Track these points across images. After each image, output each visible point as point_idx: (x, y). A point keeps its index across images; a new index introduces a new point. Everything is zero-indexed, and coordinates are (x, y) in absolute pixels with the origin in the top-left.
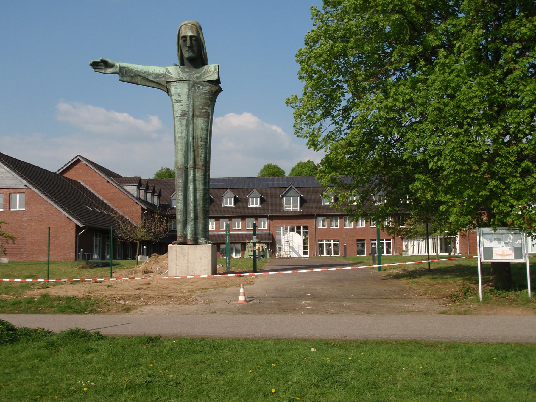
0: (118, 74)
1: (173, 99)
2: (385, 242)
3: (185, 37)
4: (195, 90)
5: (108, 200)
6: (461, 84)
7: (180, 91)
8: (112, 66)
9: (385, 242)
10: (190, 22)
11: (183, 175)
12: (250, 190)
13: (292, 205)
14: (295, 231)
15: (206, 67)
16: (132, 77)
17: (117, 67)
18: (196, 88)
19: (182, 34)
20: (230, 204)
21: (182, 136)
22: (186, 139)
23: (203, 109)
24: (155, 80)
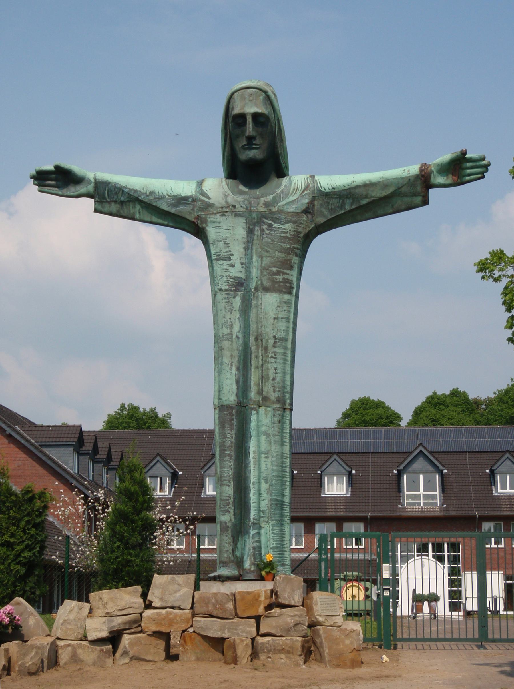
1: (213, 252)
3: (242, 117)
4: (262, 231)
7: (229, 232)
10: (245, 85)
11: (235, 422)
13: (422, 492)
14: (431, 553)
15: (285, 181)
16: (122, 203)
17: (89, 182)
18: (265, 227)
19: (237, 111)
21: (231, 334)
22: (241, 341)
23: (278, 273)
24: (173, 210)
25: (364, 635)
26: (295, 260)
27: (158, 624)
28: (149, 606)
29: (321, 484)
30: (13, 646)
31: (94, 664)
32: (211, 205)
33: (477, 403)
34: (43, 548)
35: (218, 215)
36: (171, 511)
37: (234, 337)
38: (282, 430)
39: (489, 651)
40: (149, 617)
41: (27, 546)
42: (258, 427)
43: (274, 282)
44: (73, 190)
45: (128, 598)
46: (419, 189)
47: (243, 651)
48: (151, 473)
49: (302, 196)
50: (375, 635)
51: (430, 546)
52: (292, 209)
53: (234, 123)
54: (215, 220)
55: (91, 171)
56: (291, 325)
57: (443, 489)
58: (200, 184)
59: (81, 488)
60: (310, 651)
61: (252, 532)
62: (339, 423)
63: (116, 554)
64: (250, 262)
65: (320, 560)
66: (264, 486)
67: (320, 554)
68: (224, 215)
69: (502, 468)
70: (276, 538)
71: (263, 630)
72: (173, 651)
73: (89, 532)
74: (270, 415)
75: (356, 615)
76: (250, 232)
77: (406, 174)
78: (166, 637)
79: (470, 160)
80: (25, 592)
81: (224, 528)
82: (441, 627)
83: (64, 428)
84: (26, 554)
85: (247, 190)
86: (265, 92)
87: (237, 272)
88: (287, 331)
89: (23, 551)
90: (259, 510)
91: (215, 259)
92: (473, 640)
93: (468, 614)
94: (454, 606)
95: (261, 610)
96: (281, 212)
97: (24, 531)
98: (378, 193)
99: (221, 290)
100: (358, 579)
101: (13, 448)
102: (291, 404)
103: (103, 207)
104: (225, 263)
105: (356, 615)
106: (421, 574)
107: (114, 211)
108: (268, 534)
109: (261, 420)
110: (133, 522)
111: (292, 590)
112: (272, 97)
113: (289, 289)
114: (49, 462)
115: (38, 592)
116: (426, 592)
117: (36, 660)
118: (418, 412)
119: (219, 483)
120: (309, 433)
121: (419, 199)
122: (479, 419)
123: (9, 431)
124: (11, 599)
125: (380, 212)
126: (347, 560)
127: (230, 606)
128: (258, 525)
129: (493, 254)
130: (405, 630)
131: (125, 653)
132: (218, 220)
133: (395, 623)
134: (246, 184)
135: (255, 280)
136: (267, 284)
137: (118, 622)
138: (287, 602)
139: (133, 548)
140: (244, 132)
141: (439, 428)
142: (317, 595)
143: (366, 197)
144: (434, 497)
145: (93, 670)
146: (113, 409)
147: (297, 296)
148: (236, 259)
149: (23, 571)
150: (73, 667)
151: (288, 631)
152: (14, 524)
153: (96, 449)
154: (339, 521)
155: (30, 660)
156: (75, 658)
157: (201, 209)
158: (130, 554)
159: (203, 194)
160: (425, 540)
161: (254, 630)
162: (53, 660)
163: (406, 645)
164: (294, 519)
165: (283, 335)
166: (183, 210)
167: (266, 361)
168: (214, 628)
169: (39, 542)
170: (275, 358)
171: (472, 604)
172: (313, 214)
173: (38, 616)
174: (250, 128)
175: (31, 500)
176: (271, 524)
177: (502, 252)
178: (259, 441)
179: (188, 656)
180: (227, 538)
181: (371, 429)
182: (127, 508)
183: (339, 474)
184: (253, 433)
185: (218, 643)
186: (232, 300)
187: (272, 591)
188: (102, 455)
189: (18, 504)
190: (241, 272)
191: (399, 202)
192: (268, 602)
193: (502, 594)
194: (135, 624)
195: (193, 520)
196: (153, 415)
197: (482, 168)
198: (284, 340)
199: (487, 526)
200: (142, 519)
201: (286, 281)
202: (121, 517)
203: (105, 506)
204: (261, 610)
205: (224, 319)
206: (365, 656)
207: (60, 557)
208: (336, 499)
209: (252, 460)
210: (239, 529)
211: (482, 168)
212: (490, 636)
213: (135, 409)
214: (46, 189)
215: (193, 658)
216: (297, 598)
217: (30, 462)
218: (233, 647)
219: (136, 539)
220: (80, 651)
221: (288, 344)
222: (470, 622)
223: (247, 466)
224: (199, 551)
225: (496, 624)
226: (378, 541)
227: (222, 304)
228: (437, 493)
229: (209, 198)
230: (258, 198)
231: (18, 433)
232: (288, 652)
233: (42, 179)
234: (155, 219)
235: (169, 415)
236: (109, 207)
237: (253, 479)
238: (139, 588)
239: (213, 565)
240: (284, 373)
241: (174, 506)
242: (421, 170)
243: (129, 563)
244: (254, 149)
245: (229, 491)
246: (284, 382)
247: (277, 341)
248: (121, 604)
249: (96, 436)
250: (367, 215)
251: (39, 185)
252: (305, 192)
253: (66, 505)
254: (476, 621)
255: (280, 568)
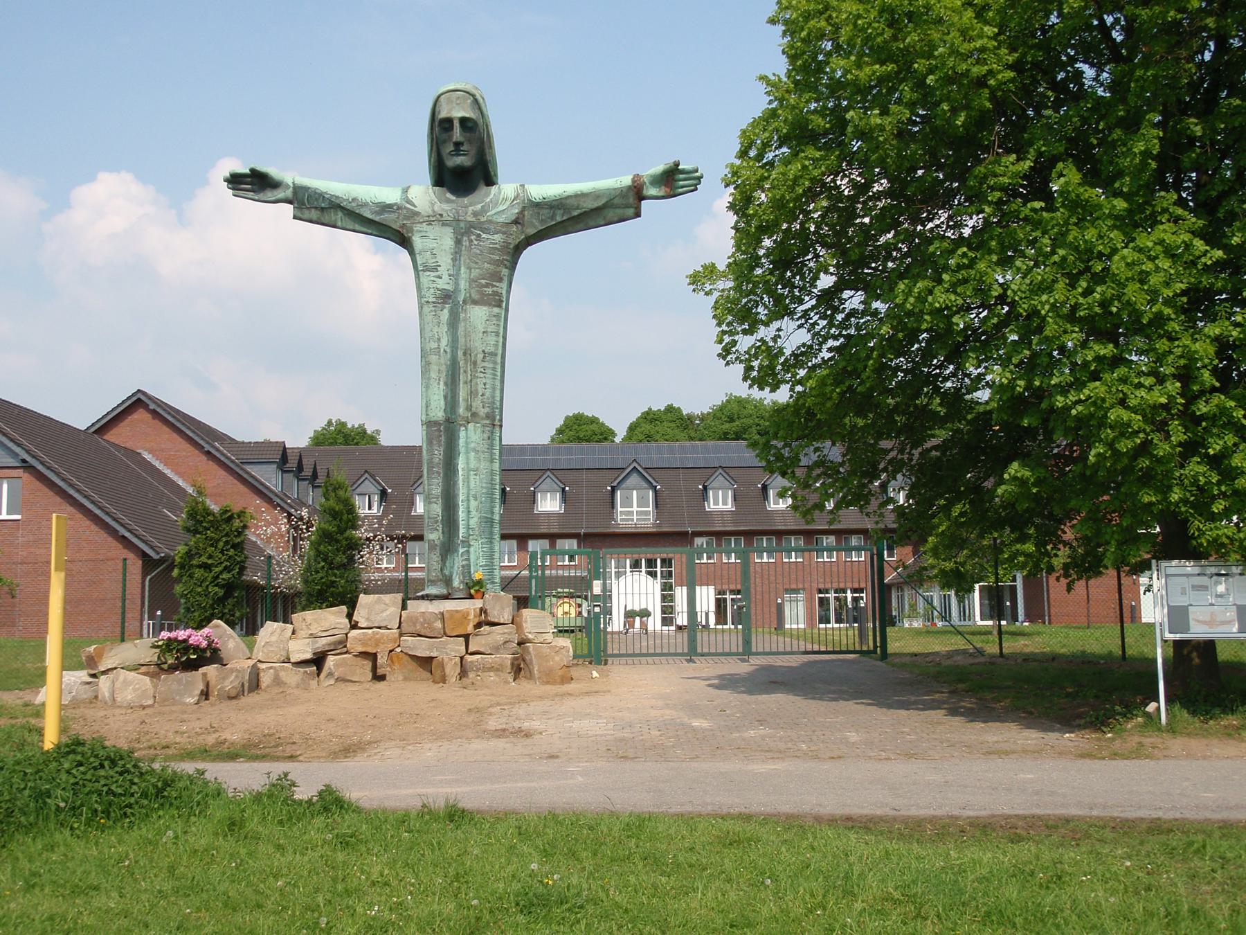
0: (290, 202)
1: (419, 262)
2: (849, 595)
3: (449, 121)
6: (1038, 233)
7: (436, 242)
9: (849, 595)
10: (459, 87)
11: (443, 439)
12: (540, 473)
13: (635, 509)
14: (643, 569)
15: (494, 189)
16: (323, 209)
17: (287, 186)
18: (473, 237)
19: (443, 114)
20: (725, 503)
22: (449, 356)
23: (487, 285)
24: (377, 219)
25: (575, 651)
26: (505, 272)
27: (364, 644)
28: (354, 626)
29: (534, 501)
30: (211, 670)
31: (297, 686)
32: (418, 214)
33: (690, 418)
34: (242, 569)
36: (378, 529)
38: (491, 447)
39: (698, 665)
40: (355, 638)
41: (226, 568)
42: (467, 443)
43: (482, 294)
44: (270, 195)
45: (331, 619)
46: (631, 200)
47: (452, 670)
48: (358, 490)
49: (512, 206)
50: (586, 652)
51: (659, 561)
52: (501, 219)
53: (440, 127)
55: (289, 175)
56: (501, 340)
57: (657, 505)
58: (405, 191)
59: (286, 506)
60: (519, 669)
61: (461, 550)
62: (553, 439)
63: (320, 575)
64: (458, 274)
65: (531, 577)
66: (473, 504)
67: (531, 571)
69: (713, 485)
70: (487, 556)
71: (471, 649)
72: (380, 672)
73: (295, 551)
74: (479, 431)
75: (566, 631)
76: (458, 242)
77: (618, 185)
78: (373, 657)
79: (683, 172)
80: (224, 614)
81: (432, 547)
82: (651, 642)
83: (267, 444)
84: (225, 576)
85: (454, 198)
86: (473, 96)
87: (444, 283)
88: (496, 346)
89: (221, 573)
90: (468, 528)
92: (682, 655)
93: (680, 628)
94: (667, 621)
95: (470, 629)
96: (490, 222)
97: (222, 552)
98: (590, 204)
100: (571, 596)
101: (212, 466)
102: (501, 420)
104: (433, 274)
105: (566, 631)
106: (633, 590)
107: (315, 218)
108: (477, 552)
109: (470, 437)
110: (337, 541)
111: (501, 606)
112: (481, 101)
113: (499, 301)
114: (250, 480)
115: (238, 614)
116: (637, 608)
117: (236, 683)
118: (632, 428)
119: (428, 500)
120: (522, 449)
121: (631, 211)
122: (693, 434)
123: (207, 447)
124: (210, 621)
125: (570, 229)
126: (557, 577)
127: (439, 625)
128: (466, 543)
129: (705, 267)
130: (616, 646)
131: (330, 674)
133: (605, 638)
134: (453, 192)
135: (463, 292)
136: (476, 296)
137: (322, 644)
138: (496, 621)
139: (338, 568)
140: (450, 137)
141: (653, 444)
142: (527, 613)
143: (578, 208)
144: (647, 513)
145: (296, 692)
146: (319, 424)
147: (507, 310)
148: (444, 270)
149: (221, 593)
150: (276, 690)
151: (497, 649)
152: (212, 545)
153: (300, 467)
154: (552, 537)
155: (230, 684)
156: (277, 681)
157: (407, 218)
158: (335, 575)
159: (409, 202)
160: (636, 556)
161: (463, 648)
162: (255, 684)
163: (616, 660)
164: (504, 537)
165: (492, 349)
166: (387, 218)
168: (422, 647)
169: (238, 563)
171: (682, 619)
172: (523, 225)
173: (238, 639)
174: (457, 134)
175: (231, 518)
177: (713, 264)
178: (468, 458)
179: (395, 676)
180: (436, 557)
181: (585, 445)
182: (332, 529)
183: (552, 491)
184: (462, 450)
185: (426, 663)
187: (481, 609)
188: (307, 472)
189: (215, 525)
191: (610, 214)
192: (477, 620)
193: (712, 607)
194: (341, 645)
195: (402, 539)
196: (362, 432)
197: (695, 180)
198: (494, 354)
199: (699, 541)
200: (346, 539)
201: (496, 293)
202: (325, 536)
203: (309, 525)
204: (470, 629)
206: (575, 672)
207: (262, 578)
208: (549, 515)
209: (461, 478)
210: (448, 548)
211: (695, 180)
212: (699, 651)
213: (344, 424)
214: (241, 193)
215: (401, 678)
216: (506, 616)
217: (231, 479)
218: (442, 666)
219: (341, 559)
220: (282, 674)
221: (497, 358)
222: (679, 635)
223: (455, 483)
224: (407, 570)
225: (705, 638)
226: (589, 558)
227: (429, 318)
228: (650, 509)
230: (467, 207)
231: (218, 450)
232: (498, 670)
233: (235, 181)
234: (357, 227)
235: (378, 432)
237: (461, 497)
238: (344, 608)
239: (421, 583)
240: (494, 389)
241: (381, 525)
242: (634, 181)
243: (335, 584)
244: (462, 158)
245: (437, 509)
246: (493, 397)
248: (326, 625)
249: (301, 453)
250: (579, 227)
251: (233, 189)
253: (268, 524)
254: (686, 635)
255: (489, 586)
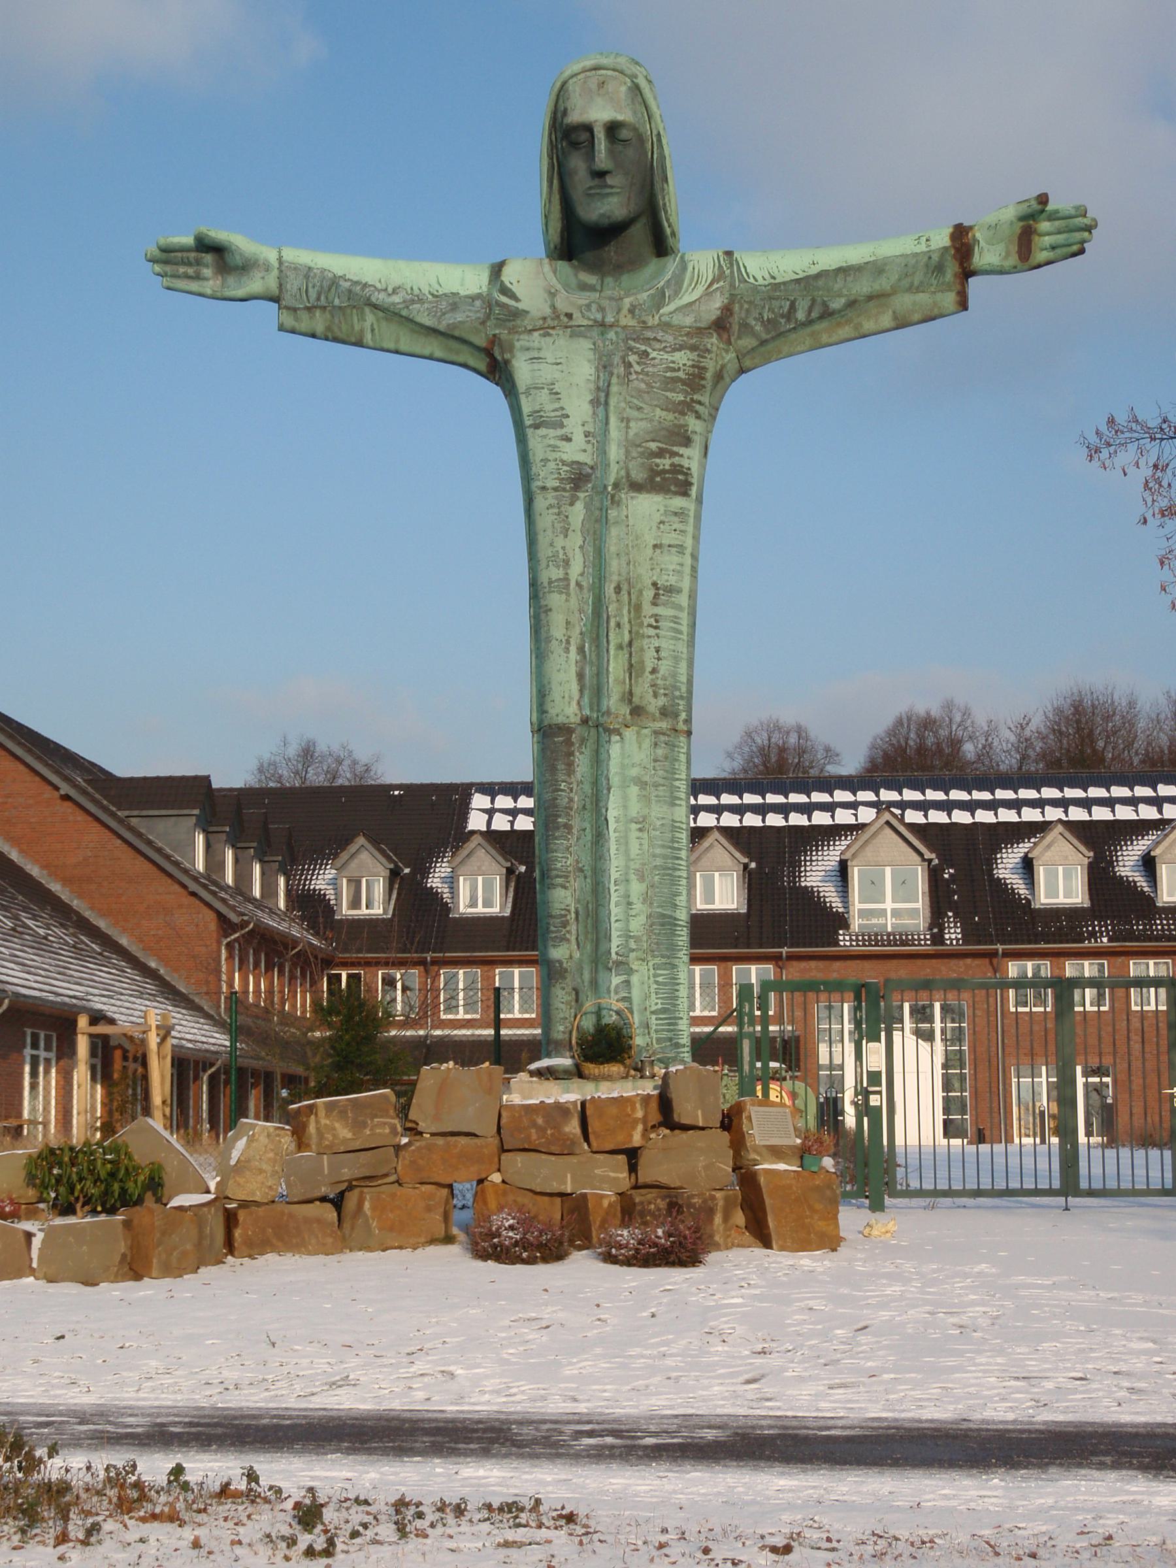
1: (526, 408)
5: (66, 881)
8: (246, 267)
13: (889, 905)
17: (268, 268)
21: (566, 579)
35: (536, 334)
37: (573, 584)
54: (531, 344)
68: (549, 335)
87: (577, 451)
91: (530, 426)
99: (544, 488)
103: (296, 319)
132: (536, 344)
167: (637, 633)
170: (656, 628)
176: (650, 964)
186: (566, 508)
190: (585, 451)
205: (550, 549)
229: (517, 300)
236: (311, 318)
247: (661, 592)
252: (715, 286)
